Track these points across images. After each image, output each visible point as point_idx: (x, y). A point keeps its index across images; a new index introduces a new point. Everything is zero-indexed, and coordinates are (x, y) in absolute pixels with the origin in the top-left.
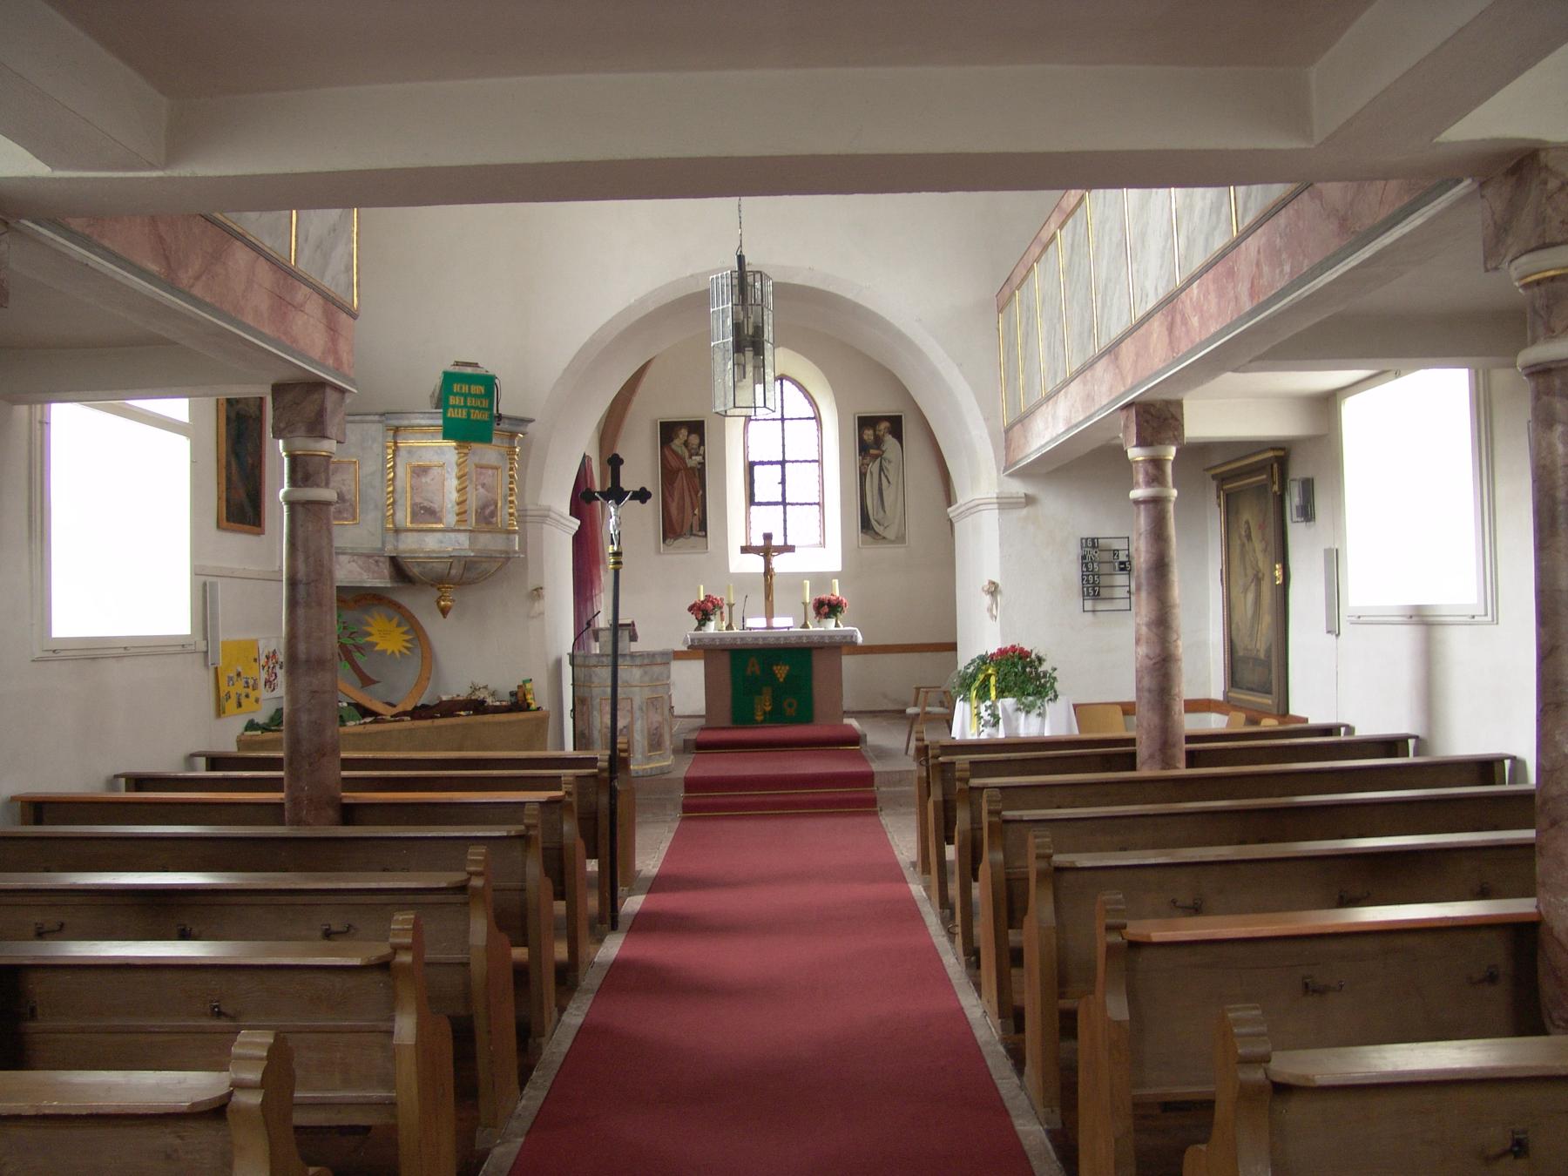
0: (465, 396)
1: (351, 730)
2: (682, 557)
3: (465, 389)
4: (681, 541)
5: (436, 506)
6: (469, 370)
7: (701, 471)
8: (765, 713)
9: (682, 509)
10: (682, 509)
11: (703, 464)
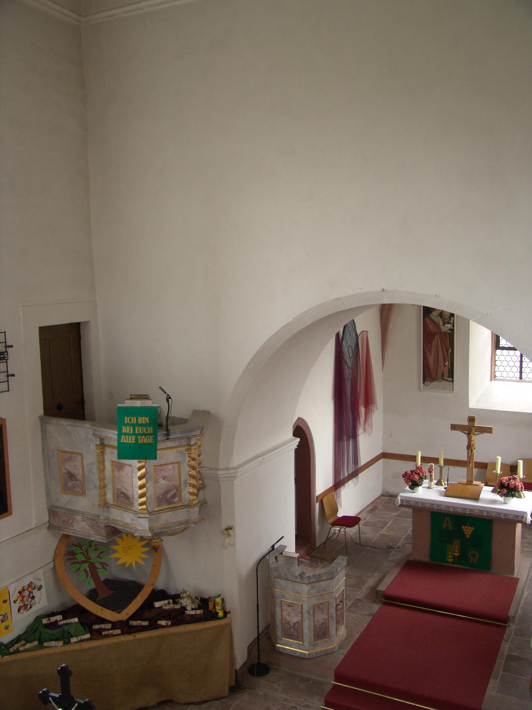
0: (134, 426)
1: (77, 647)
2: (435, 394)
3: (134, 420)
4: (435, 383)
5: (129, 494)
6: (138, 403)
7: (451, 335)
8: (454, 557)
9: (437, 361)
10: (437, 361)
11: (452, 330)
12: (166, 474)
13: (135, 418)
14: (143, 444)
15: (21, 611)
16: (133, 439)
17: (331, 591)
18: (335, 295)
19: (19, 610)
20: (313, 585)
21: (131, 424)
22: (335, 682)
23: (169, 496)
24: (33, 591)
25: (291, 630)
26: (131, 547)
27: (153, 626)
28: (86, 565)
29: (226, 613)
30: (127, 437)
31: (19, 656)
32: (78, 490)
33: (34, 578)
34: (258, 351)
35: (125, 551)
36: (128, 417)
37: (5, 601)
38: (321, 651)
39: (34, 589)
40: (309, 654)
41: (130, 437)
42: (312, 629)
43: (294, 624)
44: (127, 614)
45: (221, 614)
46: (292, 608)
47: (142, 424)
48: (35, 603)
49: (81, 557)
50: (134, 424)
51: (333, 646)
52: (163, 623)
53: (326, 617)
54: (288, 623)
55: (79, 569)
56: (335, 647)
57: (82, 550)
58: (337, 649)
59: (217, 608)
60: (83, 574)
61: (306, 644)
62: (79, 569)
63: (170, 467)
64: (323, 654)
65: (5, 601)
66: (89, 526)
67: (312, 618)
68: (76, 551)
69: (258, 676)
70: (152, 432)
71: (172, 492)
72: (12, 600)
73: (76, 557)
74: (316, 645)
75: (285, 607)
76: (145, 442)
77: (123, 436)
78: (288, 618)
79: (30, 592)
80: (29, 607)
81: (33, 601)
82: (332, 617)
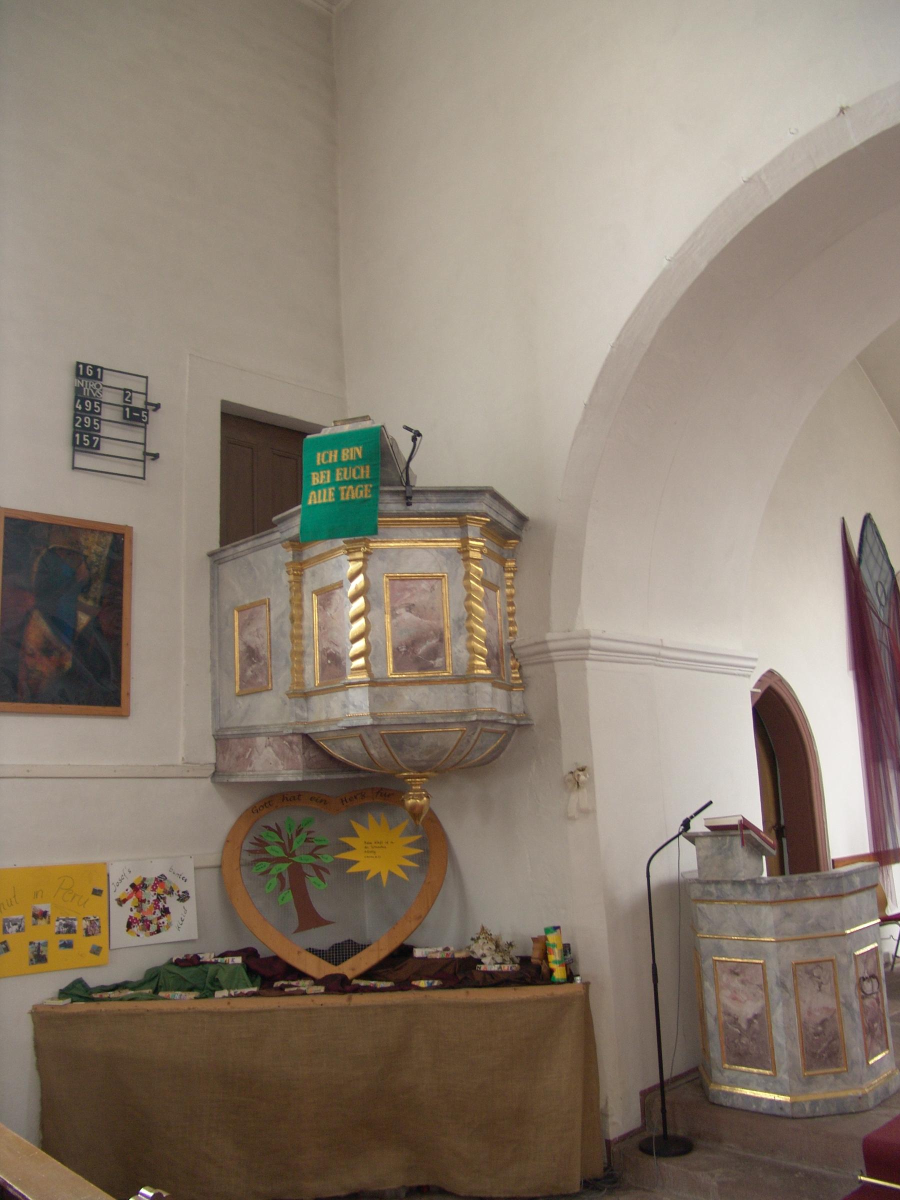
0: (332, 467)
1: (223, 1006)
3: (333, 456)
12: (415, 600)
13: (336, 452)
14: (351, 501)
15: (136, 929)
16: (331, 494)
17: (838, 931)
18: (746, 173)
19: (129, 926)
20: (790, 907)
21: (328, 464)
22: (869, 1176)
23: (421, 650)
24: (168, 897)
25: (744, 1040)
26: (383, 845)
27: (404, 985)
28: (284, 867)
29: (570, 978)
30: (320, 492)
31: (103, 1006)
32: (260, 680)
33: (171, 870)
34: (610, 356)
35: (370, 849)
36: (321, 451)
37: (97, 892)
38: (827, 1101)
39: (171, 892)
40: (792, 1104)
41: (325, 491)
42: (796, 1031)
43: (750, 1022)
44: (353, 969)
45: (559, 973)
46: (741, 977)
47: (349, 461)
48: (168, 926)
49: (276, 851)
50: (333, 463)
51: (860, 1093)
52: (423, 983)
53: (831, 1003)
54: (735, 1021)
55: (268, 871)
56: (865, 1095)
57: (281, 838)
58: (871, 1103)
59: (551, 958)
60: (274, 882)
61: (783, 1076)
62: (268, 871)
63: (424, 585)
64: (833, 1110)
65: (97, 892)
66: (277, 755)
67: (793, 1001)
68: (269, 839)
69: (660, 1154)
70: (368, 476)
71: (429, 643)
72: (114, 896)
73: (268, 849)
74: (810, 1080)
75: (725, 978)
76: (353, 497)
77: (313, 493)
78: (733, 1007)
79: (159, 898)
80: (153, 928)
81: (165, 919)
82: (849, 1007)
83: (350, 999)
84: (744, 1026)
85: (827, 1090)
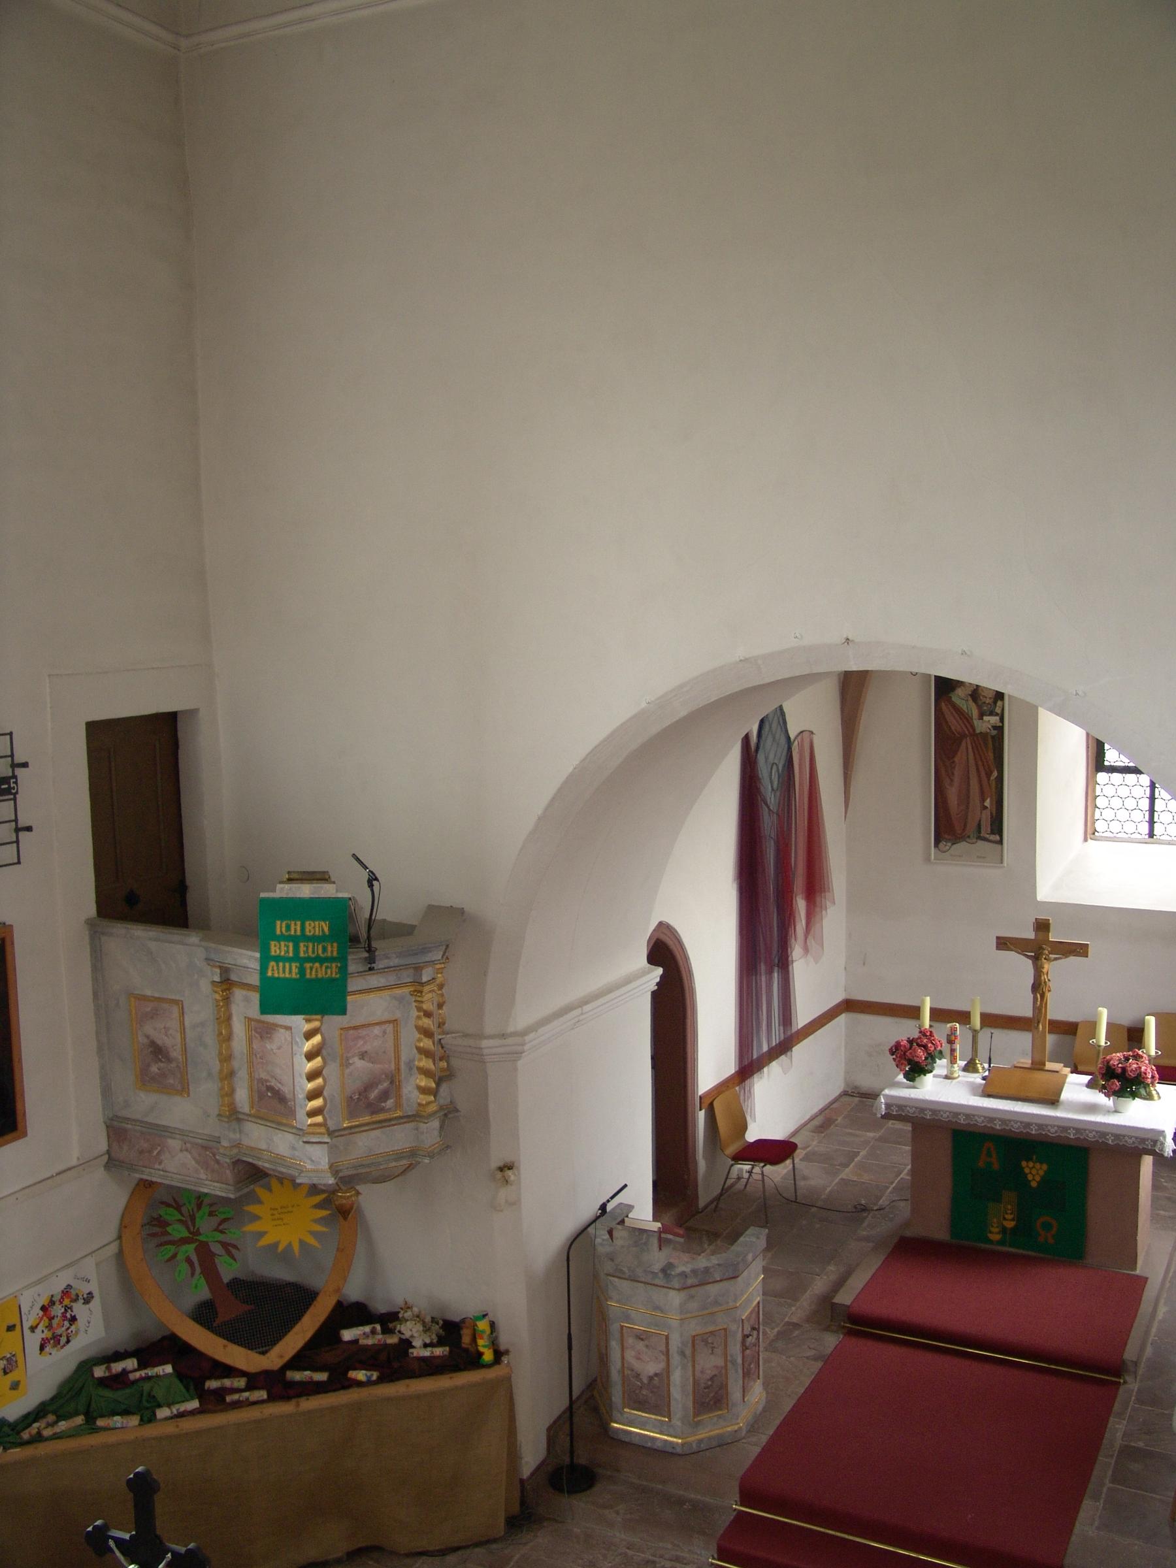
0: (295, 940)
1: (170, 1429)
2: (962, 870)
3: (296, 928)
4: (962, 846)
5: (286, 1090)
6: (305, 891)
7: (996, 739)
8: (1004, 1230)
9: (965, 798)
10: (965, 798)
11: (1000, 729)
12: (367, 1047)
13: (299, 923)
14: (317, 980)
15: (47, 1349)
16: (295, 970)
17: (731, 1304)
19: (42, 1348)
20: (693, 1291)
21: (290, 936)
22: (741, 1505)
23: (373, 1095)
24: (73, 1304)
25: (644, 1392)
26: (290, 1209)
28: (190, 1249)
29: (498, 1355)
30: (281, 964)
31: (41, 1449)
32: (171, 1081)
33: (76, 1277)
34: (571, 775)
35: (277, 1216)
36: (282, 920)
37: (11, 1328)
38: (710, 1438)
39: (76, 1300)
40: (683, 1445)
41: (287, 965)
42: (690, 1388)
43: (651, 1378)
44: (281, 1357)
45: (488, 1356)
46: (646, 1342)
47: (314, 936)
48: (77, 1333)
49: (178, 1231)
50: (296, 936)
51: (736, 1427)
52: (361, 1375)
53: (720, 1362)
54: (638, 1376)
55: (174, 1256)
56: (740, 1428)
57: (182, 1215)
58: (744, 1433)
59: (480, 1342)
60: (184, 1267)
61: (677, 1422)
62: (174, 1256)
63: (377, 1030)
64: (714, 1443)
65: (11, 1328)
66: (198, 1162)
67: (690, 1364)
68: (168, 1218)
69: (570, 1492)
70: (335, 954)
71: (380, 1087)
72: (26, 1325)
73: (169, 1229)
74: (698, 1424)
75: (630, 1341)
76: (320, 976)
77: (273, 963)
78: (637, 1365)
79: (67, 1308)
80: (63, 1340)
81: (73, 1328)
82: (734, 1362)
83: (298, 1405)
84: (646, 1381)
85: (712, 1428)
